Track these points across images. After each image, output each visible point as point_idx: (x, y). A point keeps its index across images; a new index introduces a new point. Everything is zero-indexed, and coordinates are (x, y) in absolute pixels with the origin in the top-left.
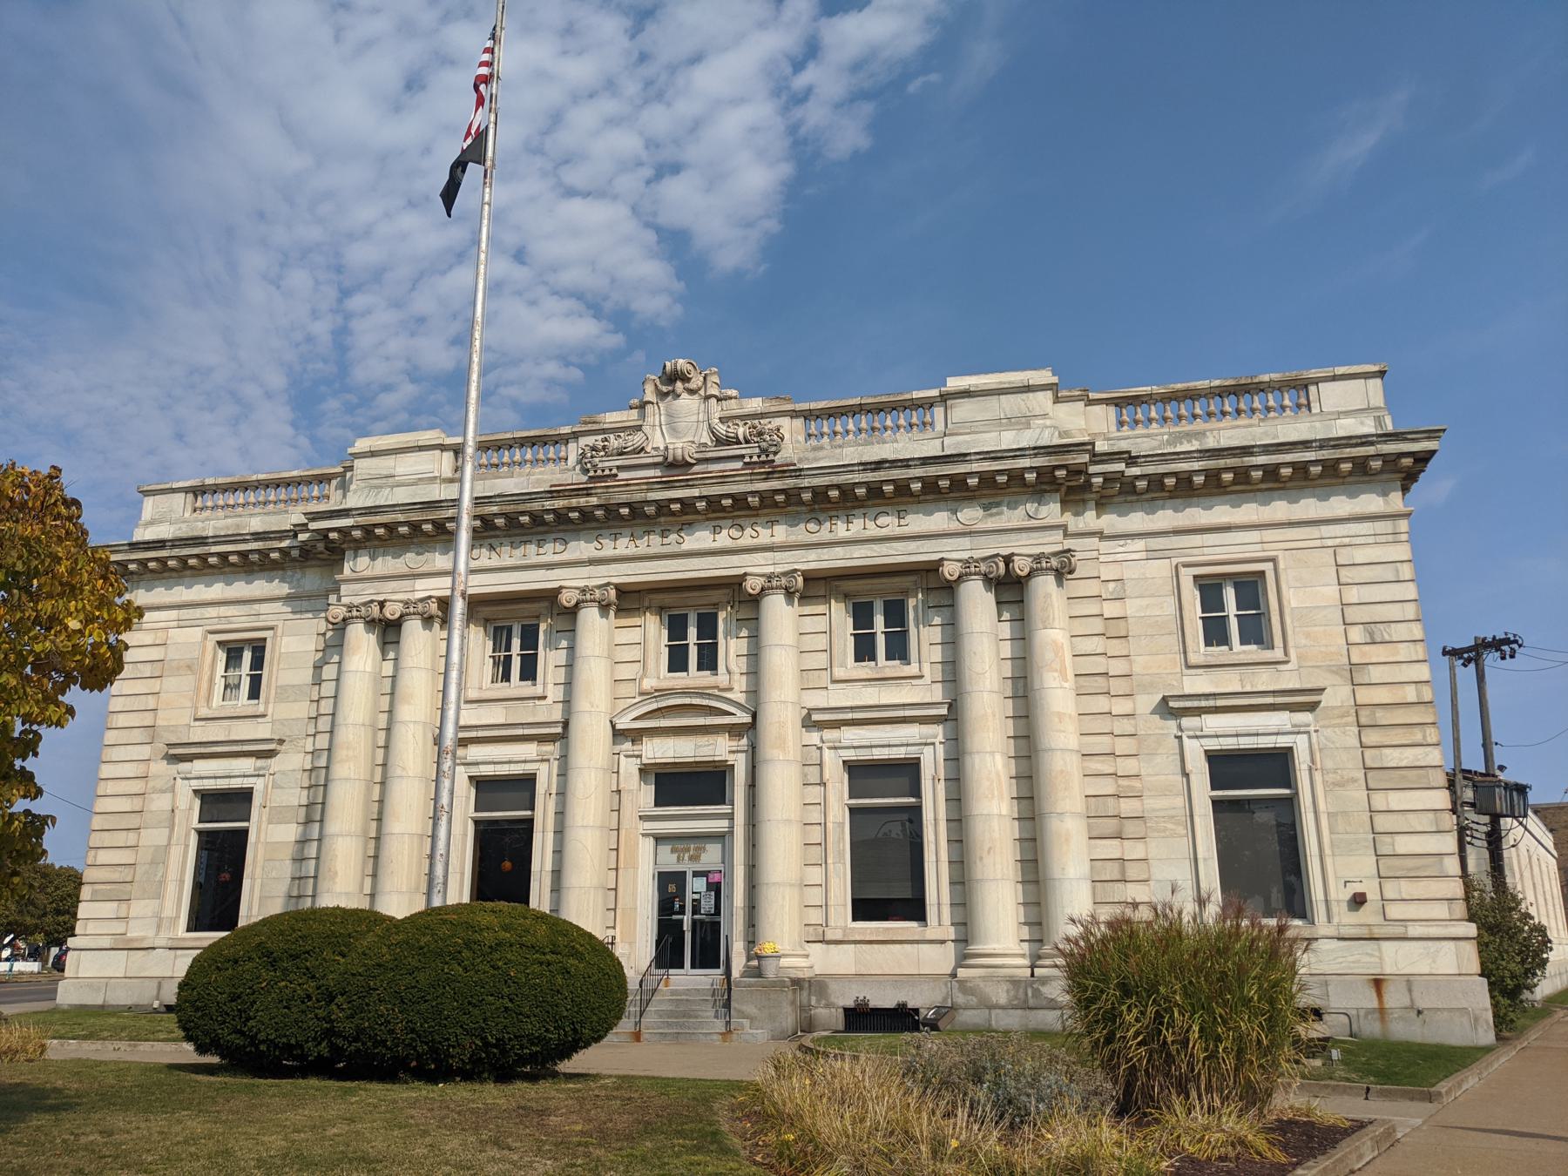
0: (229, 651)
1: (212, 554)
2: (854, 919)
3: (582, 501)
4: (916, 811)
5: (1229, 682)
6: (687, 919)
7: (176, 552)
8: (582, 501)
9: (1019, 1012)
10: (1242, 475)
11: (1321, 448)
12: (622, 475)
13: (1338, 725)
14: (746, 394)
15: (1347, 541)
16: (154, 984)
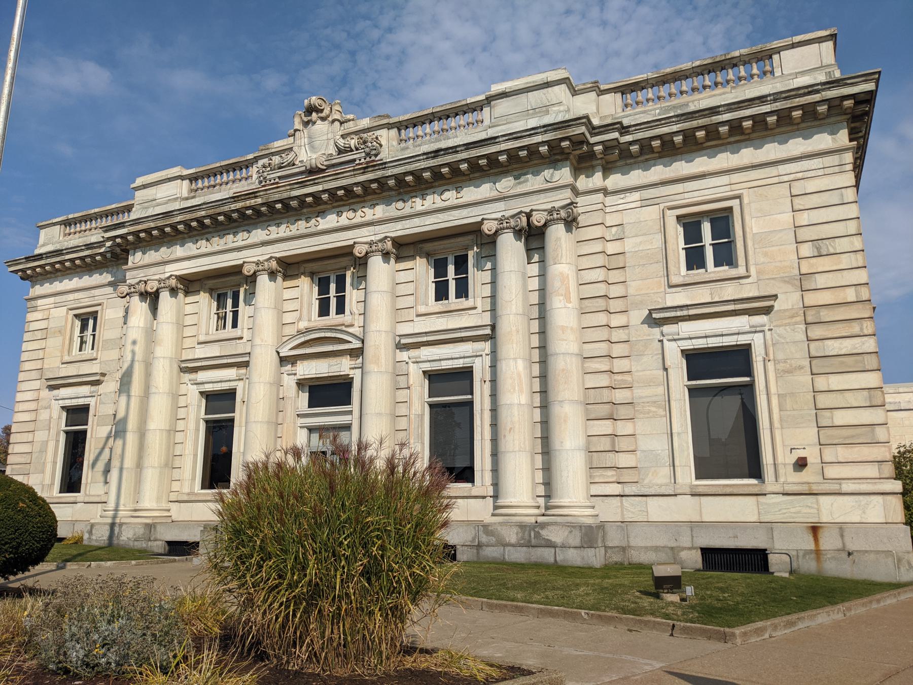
0: (685, 226)
3: (252, 202)
5: (702, 295)
9: (525, 548)
10: (712, 132)
11: (775, 100)
13: (789, 324)
15: (800, 175)
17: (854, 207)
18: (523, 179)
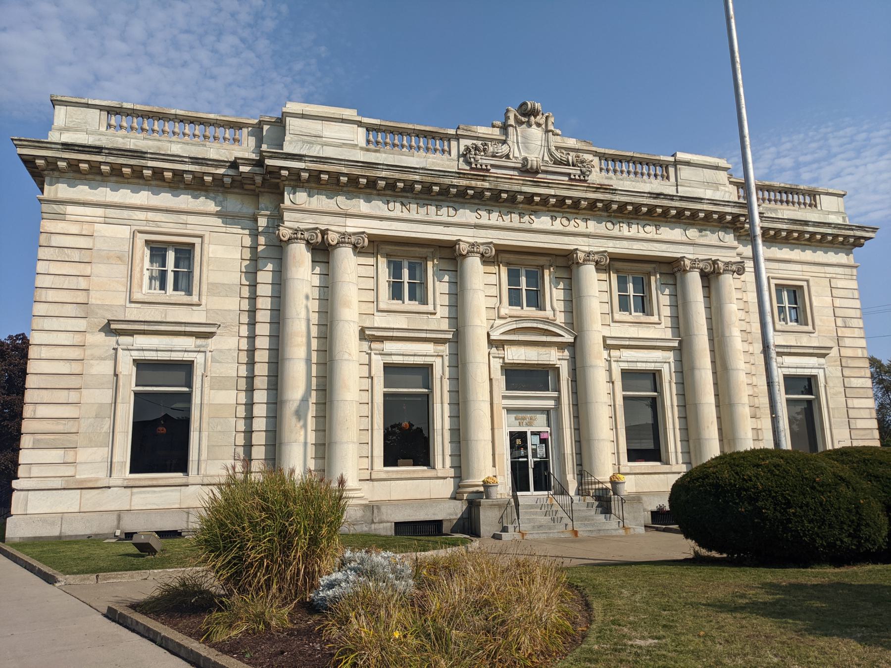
0: (152, 250)
1: (148, 168)
2: (131, 472)
3: (479, 184)
5: (399, 322)
6: (531, 461)
7: (111, 159)
8: (479, 184)
11: (834, 228)
12: (492, 170)
14: (566, 134)
16: (114, 517)
17: (858, 301)
18: (704, 233)
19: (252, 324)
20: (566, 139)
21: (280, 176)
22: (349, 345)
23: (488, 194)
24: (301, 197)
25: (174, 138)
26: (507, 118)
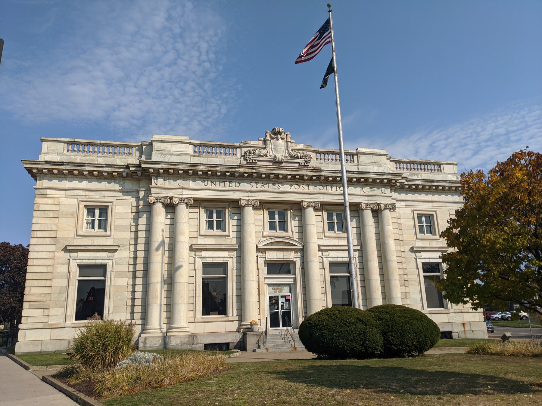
0: (88, 209)
1: (86, 171)
2: (76, 320)
3: (250, 170)
4: (225, 280)
5: (210, 241)
6: (280, 311)
7: (68, 168)
8: (250, 170)
12: (259, 163)
14: (298, 142)
16: (67, 342)
18: (373, 189)
19: (136, 244)
20: (297, 145)
21: (149, 172)
22: (184, 255)
23: (255, 175)
24: (160, 181)
25: (99, 155)
26: (266, 136)
